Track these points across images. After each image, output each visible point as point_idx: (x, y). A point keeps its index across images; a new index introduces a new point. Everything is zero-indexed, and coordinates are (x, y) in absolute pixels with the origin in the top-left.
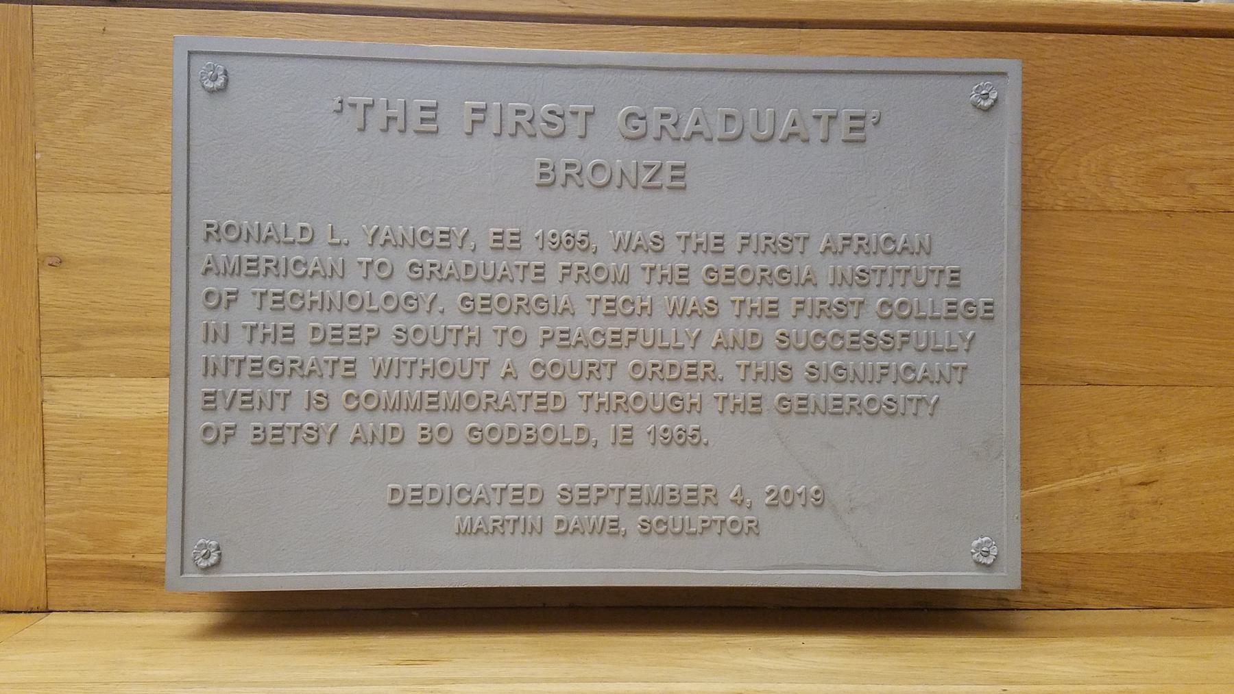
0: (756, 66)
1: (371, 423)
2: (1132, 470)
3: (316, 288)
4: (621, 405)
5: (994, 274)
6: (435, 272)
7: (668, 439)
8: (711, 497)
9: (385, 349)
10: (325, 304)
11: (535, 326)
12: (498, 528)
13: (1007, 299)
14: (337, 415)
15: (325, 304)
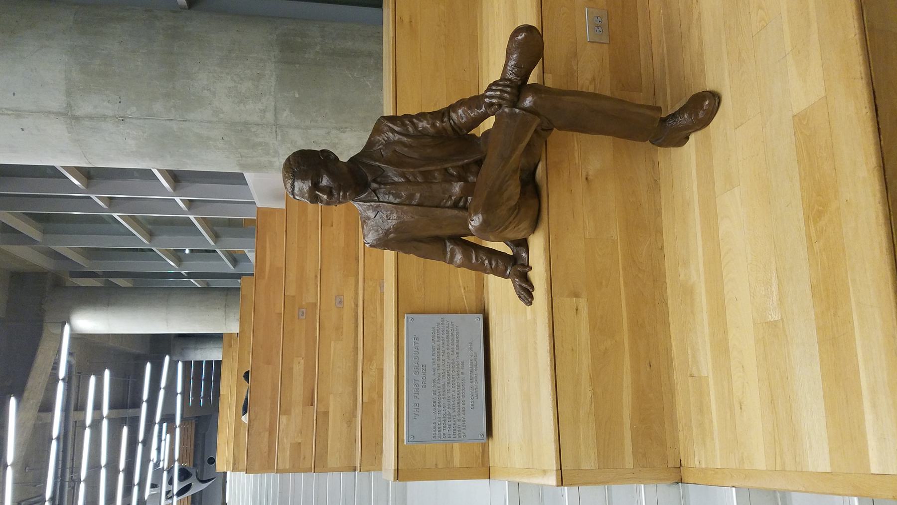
2: (463, 291)
3: (442, 422)
4: (458, 374)
5: (437, 318)
10: (445, 420)
15: (445, 420)
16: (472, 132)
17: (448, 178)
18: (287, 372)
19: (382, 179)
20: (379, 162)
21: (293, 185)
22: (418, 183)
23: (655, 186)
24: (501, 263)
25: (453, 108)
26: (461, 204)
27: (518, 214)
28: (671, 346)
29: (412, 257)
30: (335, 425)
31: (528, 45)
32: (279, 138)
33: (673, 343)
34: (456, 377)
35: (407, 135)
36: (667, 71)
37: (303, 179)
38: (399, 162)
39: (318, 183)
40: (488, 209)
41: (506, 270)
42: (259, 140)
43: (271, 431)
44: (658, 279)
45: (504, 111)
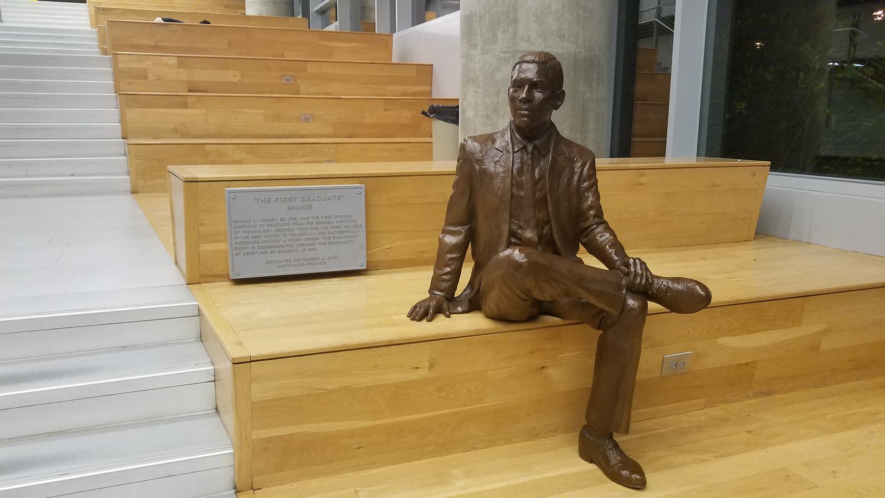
0: (308, 174)
1: (262, 250)
2: (387, 246)
3: (251, 229)
4: (303, 245)
5: (362, 220)
6: (271, 225)
7: (311, 250)
8: (318, 259)
9: (263, 239)
10: (254, 232)
11: (288, 233)
12: (284, 266)
13: (364, 224)
14: (256, 250)
15: (254, 232)
16: (581, 246)
17: (540, 225)
18: (224, 64)
19: (539, 154)
20: (554, 152)
21: (533, 62)
22: (534, 193)
23: (533, 435)
24: (444, 285)
25: (608, 229)
26: (513, 240)
27: (522, 299)
28: (378, 467)
29: (450, 191)
30: (175, 116)
31: (689, 299)
32: (502, 55)
33: (383, 469)
34: (300, 243)
35: (580, 181)
36: (643, 435)
37: (539, 73)
38: (555, 171)
39: (536, 88)
40: (533, 268)
41: (441, 291)
42: (500, 35)
43: (155, 48)
44: (446, 447)
45: (622, 278)
